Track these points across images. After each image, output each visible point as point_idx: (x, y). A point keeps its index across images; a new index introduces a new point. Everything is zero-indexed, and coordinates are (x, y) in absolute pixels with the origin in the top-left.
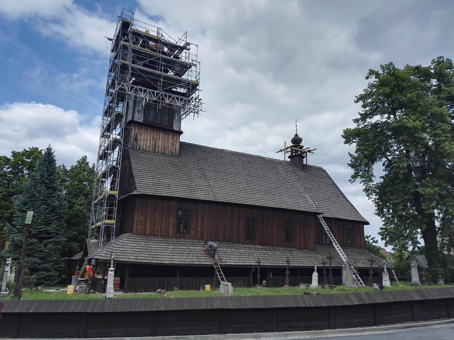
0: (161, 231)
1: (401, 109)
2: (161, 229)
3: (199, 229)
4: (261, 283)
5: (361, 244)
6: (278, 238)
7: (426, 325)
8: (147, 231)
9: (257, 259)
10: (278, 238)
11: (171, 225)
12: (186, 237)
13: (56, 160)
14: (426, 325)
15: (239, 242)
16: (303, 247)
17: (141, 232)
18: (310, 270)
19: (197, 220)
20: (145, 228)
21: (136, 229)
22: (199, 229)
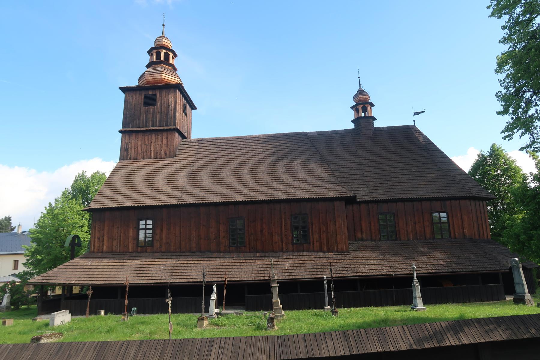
0: (120, 246)
1: (519, 81)
2: (120, 244)
3: (164, 241)
4: (129, 311)
5: (464, 233)
6: (282, 241)
7: (104, 357)
8: (105, 247)
9: (202, 277)
10: (282, 241)
11: (131, 239)
12: (148, 251)
13: (353, 121)
14: (104, 357)
15: (219, 251)
16: (325, 249)
17: (99, 250)
18: (405, 282)
19: (162, 230)
20: (103, 245)
21: (94, 246)
22: (164, 241)
